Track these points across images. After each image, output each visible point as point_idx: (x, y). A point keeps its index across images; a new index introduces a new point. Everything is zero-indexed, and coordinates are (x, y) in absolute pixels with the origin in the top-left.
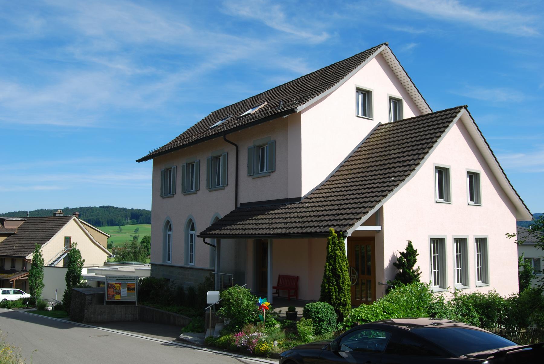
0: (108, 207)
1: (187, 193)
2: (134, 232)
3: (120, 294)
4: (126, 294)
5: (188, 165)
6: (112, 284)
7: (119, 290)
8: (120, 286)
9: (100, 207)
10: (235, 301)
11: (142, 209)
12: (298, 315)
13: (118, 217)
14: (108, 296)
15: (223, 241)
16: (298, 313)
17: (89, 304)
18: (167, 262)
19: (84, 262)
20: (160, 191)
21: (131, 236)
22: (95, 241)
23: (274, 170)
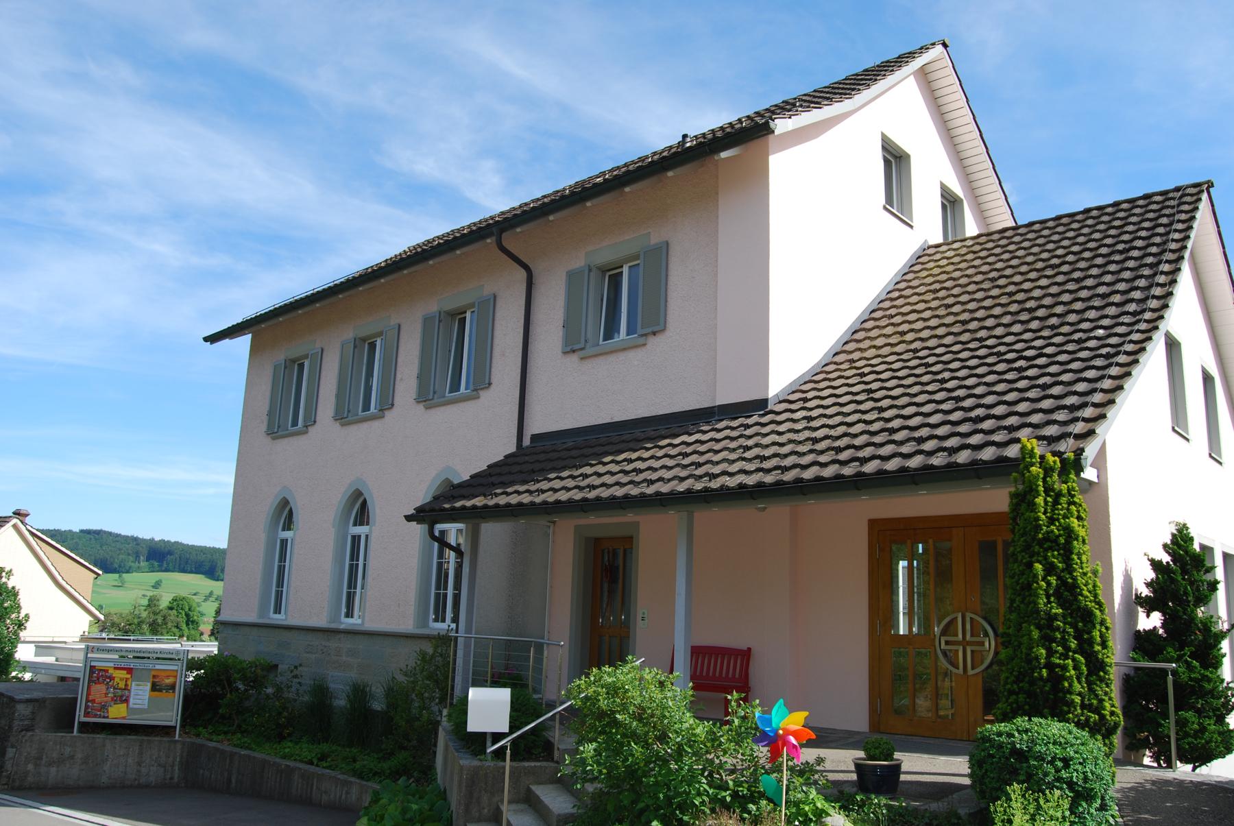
0: (98, 532)
1: (350, 418)
2: (151, 589)
3: (127, 701)
4: (147, 697)
5: (359, 342)
6: (104, 670)
7: (125, 689)
8: (129, 676)
9: (82, 531)
10: (634, 716)
11: (173, 541)
12: (903, 777)
13: (118, 555)
14: (87, 707)
15: (492, 531)
16: (904, 768)
17: (22, 731)
18: (272, 615)
19: (27, 621)
20: (265, 419)
21: (144, 595)
22: (64, 583)
23: (661, 327)
